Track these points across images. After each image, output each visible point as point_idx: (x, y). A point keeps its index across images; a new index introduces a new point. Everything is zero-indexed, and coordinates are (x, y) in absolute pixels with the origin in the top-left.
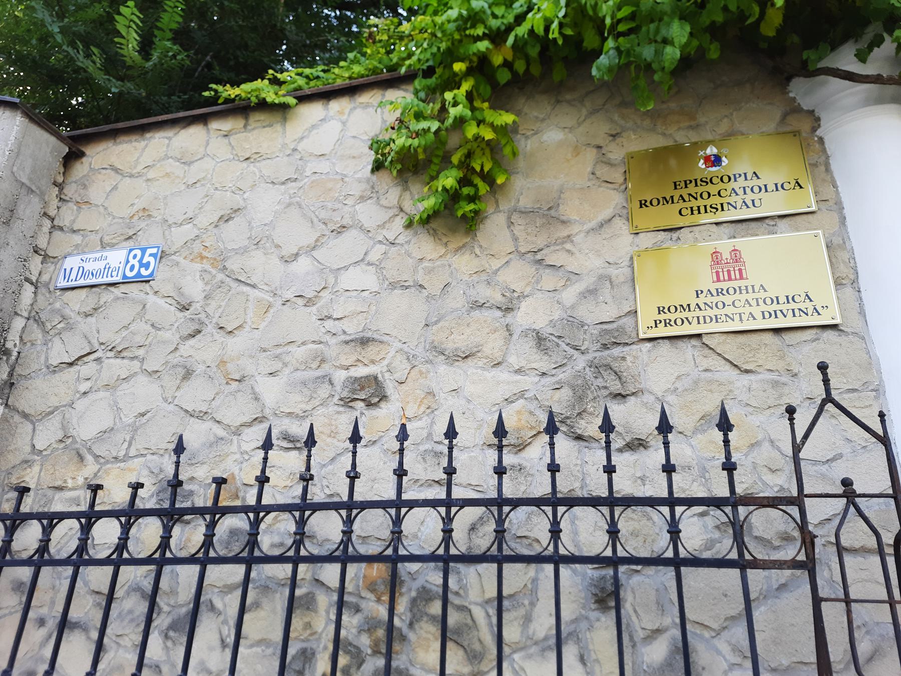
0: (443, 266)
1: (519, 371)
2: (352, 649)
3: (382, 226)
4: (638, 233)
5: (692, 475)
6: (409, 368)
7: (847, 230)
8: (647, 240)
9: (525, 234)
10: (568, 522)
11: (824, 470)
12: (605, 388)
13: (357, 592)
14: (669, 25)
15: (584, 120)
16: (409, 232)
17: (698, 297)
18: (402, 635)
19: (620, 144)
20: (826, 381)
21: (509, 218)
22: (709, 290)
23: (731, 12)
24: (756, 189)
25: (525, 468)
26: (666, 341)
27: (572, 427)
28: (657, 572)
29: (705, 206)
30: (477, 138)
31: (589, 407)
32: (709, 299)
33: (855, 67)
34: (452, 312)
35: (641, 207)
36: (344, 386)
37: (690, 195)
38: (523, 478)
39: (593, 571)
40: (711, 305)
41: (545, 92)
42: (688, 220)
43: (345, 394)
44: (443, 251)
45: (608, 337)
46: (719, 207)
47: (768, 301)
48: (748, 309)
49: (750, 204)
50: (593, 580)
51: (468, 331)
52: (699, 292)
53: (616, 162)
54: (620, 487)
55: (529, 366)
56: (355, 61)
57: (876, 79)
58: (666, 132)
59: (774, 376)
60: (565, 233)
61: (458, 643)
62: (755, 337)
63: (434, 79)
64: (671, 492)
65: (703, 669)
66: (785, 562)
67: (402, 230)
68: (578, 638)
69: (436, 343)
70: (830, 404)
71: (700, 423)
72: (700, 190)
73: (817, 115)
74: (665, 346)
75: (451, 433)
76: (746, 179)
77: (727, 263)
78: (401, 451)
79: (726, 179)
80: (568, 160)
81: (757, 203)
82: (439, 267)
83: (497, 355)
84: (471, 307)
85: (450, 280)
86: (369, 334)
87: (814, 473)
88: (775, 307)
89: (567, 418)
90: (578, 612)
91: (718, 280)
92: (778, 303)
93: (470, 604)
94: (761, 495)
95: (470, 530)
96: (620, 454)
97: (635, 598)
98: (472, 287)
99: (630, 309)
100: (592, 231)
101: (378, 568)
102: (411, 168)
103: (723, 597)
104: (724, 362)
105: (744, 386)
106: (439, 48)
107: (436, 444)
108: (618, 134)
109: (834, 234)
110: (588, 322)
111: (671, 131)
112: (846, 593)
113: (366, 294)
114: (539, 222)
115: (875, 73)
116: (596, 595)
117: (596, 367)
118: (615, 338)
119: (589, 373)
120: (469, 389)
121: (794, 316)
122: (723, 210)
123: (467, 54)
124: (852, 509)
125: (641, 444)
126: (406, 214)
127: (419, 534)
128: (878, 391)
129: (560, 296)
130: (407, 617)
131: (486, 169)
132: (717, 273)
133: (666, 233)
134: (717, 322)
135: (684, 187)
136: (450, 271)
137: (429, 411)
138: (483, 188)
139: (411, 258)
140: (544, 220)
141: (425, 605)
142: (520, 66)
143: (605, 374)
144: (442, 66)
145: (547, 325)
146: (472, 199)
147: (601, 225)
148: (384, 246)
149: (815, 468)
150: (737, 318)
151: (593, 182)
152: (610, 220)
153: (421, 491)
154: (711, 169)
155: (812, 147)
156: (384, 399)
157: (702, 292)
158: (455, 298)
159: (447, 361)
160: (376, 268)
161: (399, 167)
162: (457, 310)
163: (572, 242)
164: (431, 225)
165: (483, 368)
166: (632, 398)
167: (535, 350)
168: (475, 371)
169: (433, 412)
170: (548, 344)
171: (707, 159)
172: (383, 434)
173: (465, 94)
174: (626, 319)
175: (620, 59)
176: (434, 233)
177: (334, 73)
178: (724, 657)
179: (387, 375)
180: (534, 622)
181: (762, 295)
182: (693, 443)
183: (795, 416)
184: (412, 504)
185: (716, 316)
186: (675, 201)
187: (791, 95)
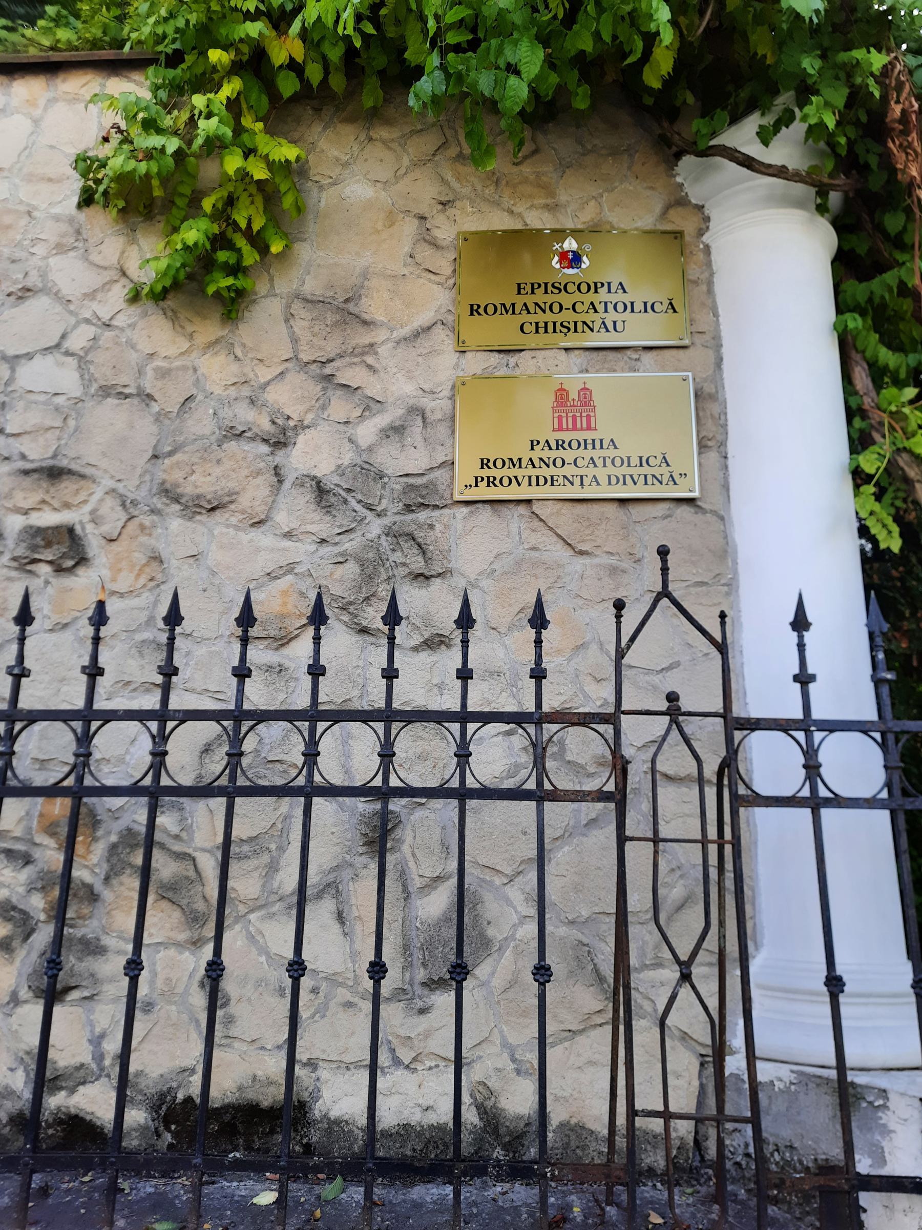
0: (184, 368)
1: (288, 535)
2: (16, 915)
3: (91, 295)
4: (464, 352)
5: (502, 683)
6: (124, 520)
7: (722, 376)
8: (475, 363)
9: (309, 334)
10: (339, 742)
11: (657, 681)
12: (404, 564)
13: (29, 837)
14: (516, 43)
15: (406, 174)
16: (135, 310)
17: (532, 449)
18: (92, 893)
19: (452, 218)
20: (665, 570)
21: (288, 306)
22: (547, 441)
23: (604, 42)
24: (620, 307)
25: (287, 669)
26: (487, 506)
27: (356, 617)
28: (445, 806)
29: (555, 323)
30: (244, 175)
31: (380, 589)
32: (546, 454)
33: (754, 149)
34: (195, 440)
35: (472, 314)
36: (19, 541)
37: (536, 304)
38: (283, 684)
39: (366, 805)
40: (547, 461)
41: (351, 119)
42: (532, 340)
43: (20, 552)
44: (186, 345)
45: (413, 496)
46: (572, 326)
47: (618, 462)
48: (591, 471)
49: (611, 327)
50: (364, 816)
51: (217, 471)
52: (535, 443)
53: (444, 244)
54: (411, 697)
55: (303, 529)
56: (57, 21)
57: (780, 172)
58: (514, 208)
59: (612, 560)
60: (367, 340)
61: (174, 903)
62: (596, 507)
63: (179, 71)
64: (464, 704)
65: (489, 923)
66: (590, 793)
67: (124, 305)
68: (337, 891)
69: (168, 486)
70: (666, 599)
71: (518, 617)
72: (550, 298)
73: (707, 212)
74: (486, 513)
75: (174, 617)
76: (609, 291)
77: (574, 406)
78: (96, 640)
79: (584, 288)
80: (378, 232)
81: (619, 327)
82: (178, 369)
83: (258, 509)
84: (225, 436)
85: (194, 392)
86: (64, 463)
87: (645, 685)
88: (625, 470)
89: (350, 603)
90: (340, 858)
91: (560, 429)
92: (629, 465)
93: (195, 850)
94: (581, 710)
95: (202, 753)
96: (415, 653)
97: (415, 838)
98: (227, 404)
99: (445, 459)
100: (403, 342)
101: (62, 804)
102: (141, 209)
103: (521, 836)
104: (555, 539)
105: (576, 572)
106: (187, 21)
107: (159, 632)
108: (449, 201)
109: (705, 380)
110: (389, 472)
111: (519, 208)
112: (656, 831)
113: (60, 400)
114: (330, 318)
115: (779, 164)
116: (365, 835)
117: (395, 536)
118: (423, 497)
119: (385, 543)
120: (215, 556)
121: (646, 483)
122: (576, 331)
123: (231, 38)
124: (675, 733)
125: (442, 642)
126: (132, 281)
127: (128, 757)
128: (731, 586)
129: (353, 432)
130: (102, 870)
131: (256, 227)
132: (560, 418)
133: (502, 356)
134: (552, 484)
135: (530, 292)
136: (194, 378)
137: (152, 584)
138: (250, 257)
139: (137, 351)
140: (338, 317)
141: (129, 853)
142: (314, 73)
143: (405, 546)
144: (195, 51)
145: (332, 472)
146: (235, 270)
147: (417, 335)
148: (93, 328)
149: (647, 678)
150: (577, 481)
151: (411, 269)
152: (429, 328)
153: (133, 698)
154: (566, 271)
155: (695, 258)
156: (83, 562)
157: (538, 442)
158: (199, 421)
159: (184, 513)
160: (79, 361)
161: (121, 204)
162: (203, 437)
163: (376, 353)
164: (169, 303)
165: (237, 528)
166: (438, 580)
167: (313, 507)
168: (225, 530)
169: (158, 586)
170: (333, 500)
171: (563, 255)
172: (79, 614)
173: (225, 102)
174: (439, 472)
175: (447, 86)
176: (173, 317)
177: (23, 36)
178: (515, 908)
179: (90, 528)
180: (281, 873)
181: (611, 453)
182: (507, 642)
183: (623, 612)
184: (109, 716)
185: (552, 477)
186: (517, 311)
187: (679, 179)
